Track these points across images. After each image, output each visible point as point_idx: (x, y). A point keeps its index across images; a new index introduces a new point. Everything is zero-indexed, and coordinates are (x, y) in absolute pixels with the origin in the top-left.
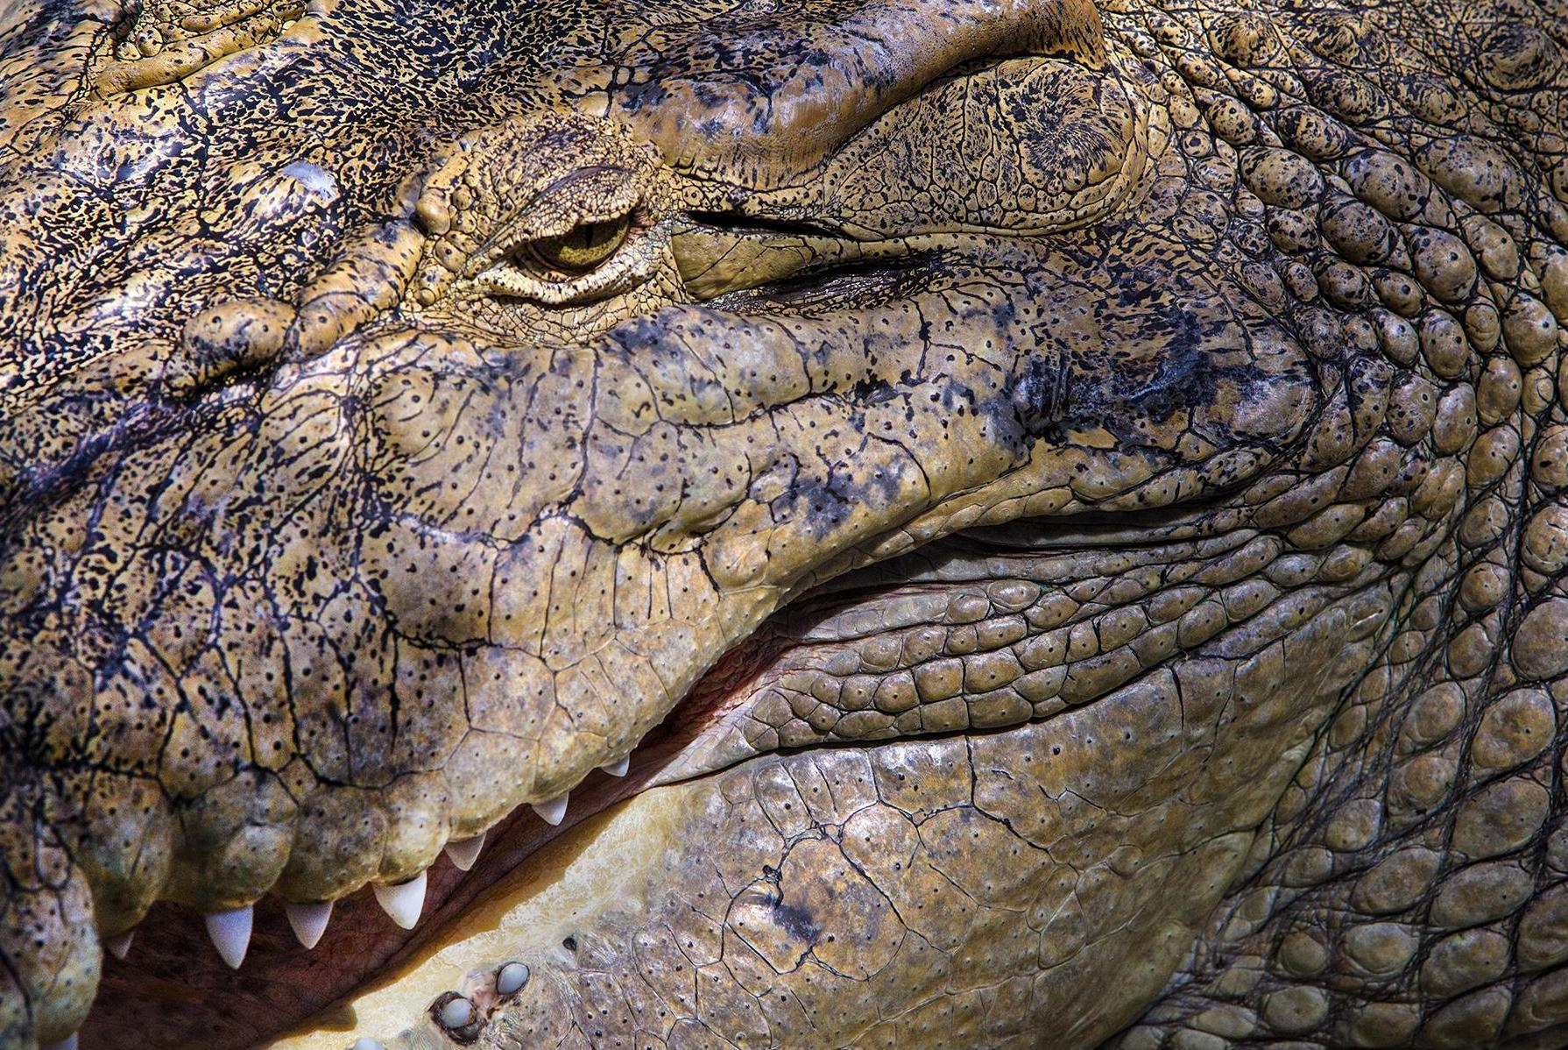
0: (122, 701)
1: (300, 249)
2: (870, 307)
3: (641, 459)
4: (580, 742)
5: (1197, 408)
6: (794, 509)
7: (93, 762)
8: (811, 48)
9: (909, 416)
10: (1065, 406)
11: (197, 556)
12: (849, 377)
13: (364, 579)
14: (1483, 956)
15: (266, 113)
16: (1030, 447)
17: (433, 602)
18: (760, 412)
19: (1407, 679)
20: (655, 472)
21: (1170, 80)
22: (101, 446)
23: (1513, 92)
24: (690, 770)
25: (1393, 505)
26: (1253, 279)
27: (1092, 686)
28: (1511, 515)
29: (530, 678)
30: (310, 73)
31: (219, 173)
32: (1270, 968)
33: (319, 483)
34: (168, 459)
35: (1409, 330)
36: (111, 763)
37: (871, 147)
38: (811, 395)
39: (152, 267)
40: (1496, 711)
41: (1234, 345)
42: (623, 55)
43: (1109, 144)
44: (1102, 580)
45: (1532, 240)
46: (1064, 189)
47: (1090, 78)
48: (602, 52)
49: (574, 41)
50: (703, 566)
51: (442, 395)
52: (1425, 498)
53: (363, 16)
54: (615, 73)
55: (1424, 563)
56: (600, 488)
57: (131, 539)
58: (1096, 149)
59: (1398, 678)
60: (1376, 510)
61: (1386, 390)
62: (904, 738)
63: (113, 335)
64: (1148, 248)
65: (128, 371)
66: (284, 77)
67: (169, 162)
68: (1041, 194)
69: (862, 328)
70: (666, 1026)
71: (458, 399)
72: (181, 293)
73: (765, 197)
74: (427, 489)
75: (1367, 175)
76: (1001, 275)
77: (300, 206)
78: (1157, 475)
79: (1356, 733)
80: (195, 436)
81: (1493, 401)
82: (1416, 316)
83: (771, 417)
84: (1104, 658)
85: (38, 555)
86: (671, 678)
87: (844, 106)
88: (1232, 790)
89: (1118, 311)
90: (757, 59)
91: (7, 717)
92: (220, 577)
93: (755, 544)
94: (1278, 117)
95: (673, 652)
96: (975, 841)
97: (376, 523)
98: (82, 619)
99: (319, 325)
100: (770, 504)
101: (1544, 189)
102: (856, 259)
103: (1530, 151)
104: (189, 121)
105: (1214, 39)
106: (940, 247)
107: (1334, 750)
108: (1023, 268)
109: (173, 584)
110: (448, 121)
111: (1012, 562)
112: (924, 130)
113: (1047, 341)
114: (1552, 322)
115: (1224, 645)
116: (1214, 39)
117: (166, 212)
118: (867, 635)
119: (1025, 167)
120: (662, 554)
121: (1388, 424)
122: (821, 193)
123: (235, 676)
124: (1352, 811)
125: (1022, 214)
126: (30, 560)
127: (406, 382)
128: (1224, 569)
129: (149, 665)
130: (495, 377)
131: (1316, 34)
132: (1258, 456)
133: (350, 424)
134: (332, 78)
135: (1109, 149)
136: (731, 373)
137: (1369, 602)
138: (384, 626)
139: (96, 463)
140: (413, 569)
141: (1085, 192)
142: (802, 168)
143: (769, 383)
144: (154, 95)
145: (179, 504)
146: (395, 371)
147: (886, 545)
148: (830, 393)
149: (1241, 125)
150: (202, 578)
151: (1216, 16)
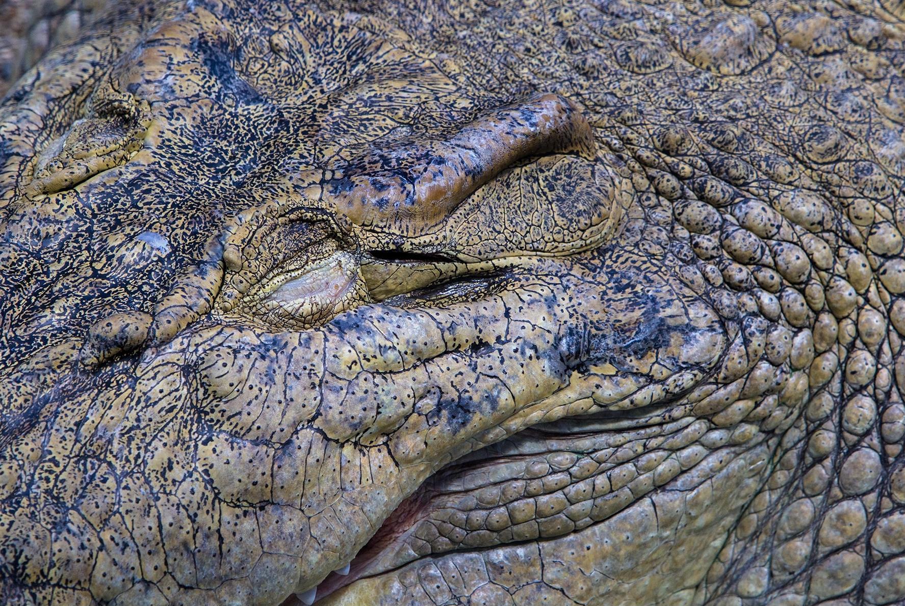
0: (68, 546)
1: (151, 282)
2: (474, 300)
3: (353, 393)
4: (324, 557)
5: (660, 350)
6: (439, 418)
7: (52, 583)
8: (435, 155)
9: (502, 362)
10: (588, 352)
11: (104, 460)
12: (467, 341)
13: (200, 469)
15: (125, 205)
16: (569, 377)
17: (240, 481)
18: (418, 363)
19: (779, 498)
20: (362, 400)
21: (632, 164)
22: (46, 400)
23: (824, 164)
24: (380, 568)
25: (771, 400)
26: (686, 275)
27: (607, 510)
28: (835, 402)
29: (295, 521)
30: (148, 181)
31: (101, 240)
33: (171, 415)
34: (85, 406)
35: (775, 300)
36: (63, 583)
37: (470, 209)
38: (446, 352)
39: (67, 296)
40: (832, 513)
41: (678, 313)
42: (327, 163)
43: (602, 202)
44: (611, 450)
45: (839, 247)
46: (579, 229)
47: (588, 165)
48: (314, 162)
49: (297, 156)
50: (390, 452)
51: (239, 362)
52: (788, 395)
53: (175, 147)
54: (324, 174)
55: (787, 431)
56: (331, 411)
57: (67, 453)
58: (595, 205)
59: (774, 497)
60: (761, 402)
61: (764, 335)
62: (503, 545)
63: (48, 336)
64: (627, 260)
65: (59, 356)
66: (133, 184)
67: (71, 235)
68: (566, 232)
69: (473, 313)
71: (248, 364)
72: (85, 310)
73: (414, 241)
74: (233, 416)
75: (746, 214)
76: (548, 279)
77: (149, 257)
78: (640, 389)
79: (751, 530)
80: (100, 392)
81: (822, 338)
82: (778, 293)
83: (425, 366)
84: (614, 494)
85: (15, 464)
86: (374, 517)
87: (456, 187)
88: (684, 566)
89: (613, 297)
90: (404, 162)
91: (3, 559)
92: (118, 472)
93: (418, 438)
94: (694, 183)
95: (374, 502)
96: (545, 602)
97: (205, 437)
99: (167, 325)
100: (426, 415)
101: (845, 218)
102: (465, 273)
103: (836, 196)
104: (81, 211)
105: (656, 141)
106: (512, 265)
107: (739, 540)
108: (559, 274)
109: (92, 477)
110: (229, 205)
111: (561, 442)
112: (499, 199)
113: (576, 315)
114: (854, 292)
115: (679, 483)
116: (656, 141)
117: (72, 264)
118: (480, 487)
119: (556, 216)
120: (366, 447)
121: (766, 354)
122: (445, 237)
123: (130, 529)
124: (752, 574)
125: (556, 244)
126: (11, 468)
127: (218, 355)
128: (678, 440)
129: (81, 525)
130: (268, 350)
131: (712, 136)
132: (695, 375)
133: (187, 381)
134: (161, 183)
135: (602, 205)
136: (402, 342)
137: (758, 455)
138: (213, 496)
139: (43, 410)
140: (228, 462)
141: (590, 230)
142: (433, 224)
143: (423, 346)
144: (60, 197)
145: (93, 431)
146: (211, 349)
147: (491, 436)
148: (457, 350)
149: (674, 188)
150: (109, 473)
151: (656, 127)
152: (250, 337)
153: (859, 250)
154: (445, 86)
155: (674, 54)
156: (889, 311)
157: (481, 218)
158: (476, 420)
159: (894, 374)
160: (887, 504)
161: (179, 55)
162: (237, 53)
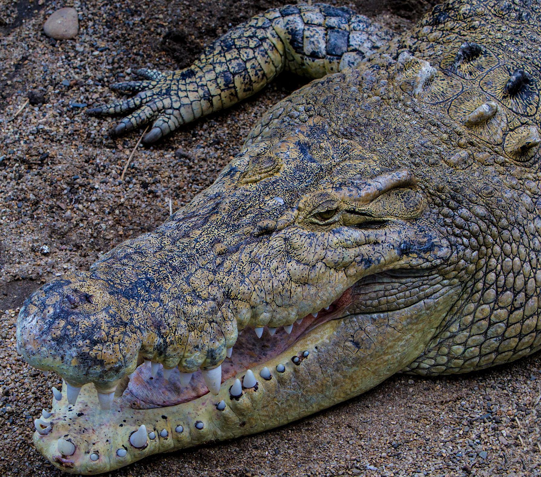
4: (322, 303)
8: (368, 183)
10: (409, 249)
14: (475, 352)
20: (338, 255)
25: (463, 272)
32: (437, 353)
33: (279, 253)
38: (366, 244)
40: (480, 308)
51: (302, 239)
59: (463, 302)
66: (274, 182)
69: (375, 232)
70: (333, 363)
71: (304, 240)
81: (482, 254)
82: (469, 238)
85: (231, 262)
86: (338, 292)
98: (238, 274)
109: (254, 269)
115: (433, 296)
124: (454, 325)
148: (369, 244)
152: (306, 232)
153: (495, 226)
154: (373, 164)
155: (442, 161)
156: (502, 246)
157: (380, 204)
158: (373, 266)
159: (502, 266)
160: (496, 306)
161: (292, 146)
162: (309, 147)
